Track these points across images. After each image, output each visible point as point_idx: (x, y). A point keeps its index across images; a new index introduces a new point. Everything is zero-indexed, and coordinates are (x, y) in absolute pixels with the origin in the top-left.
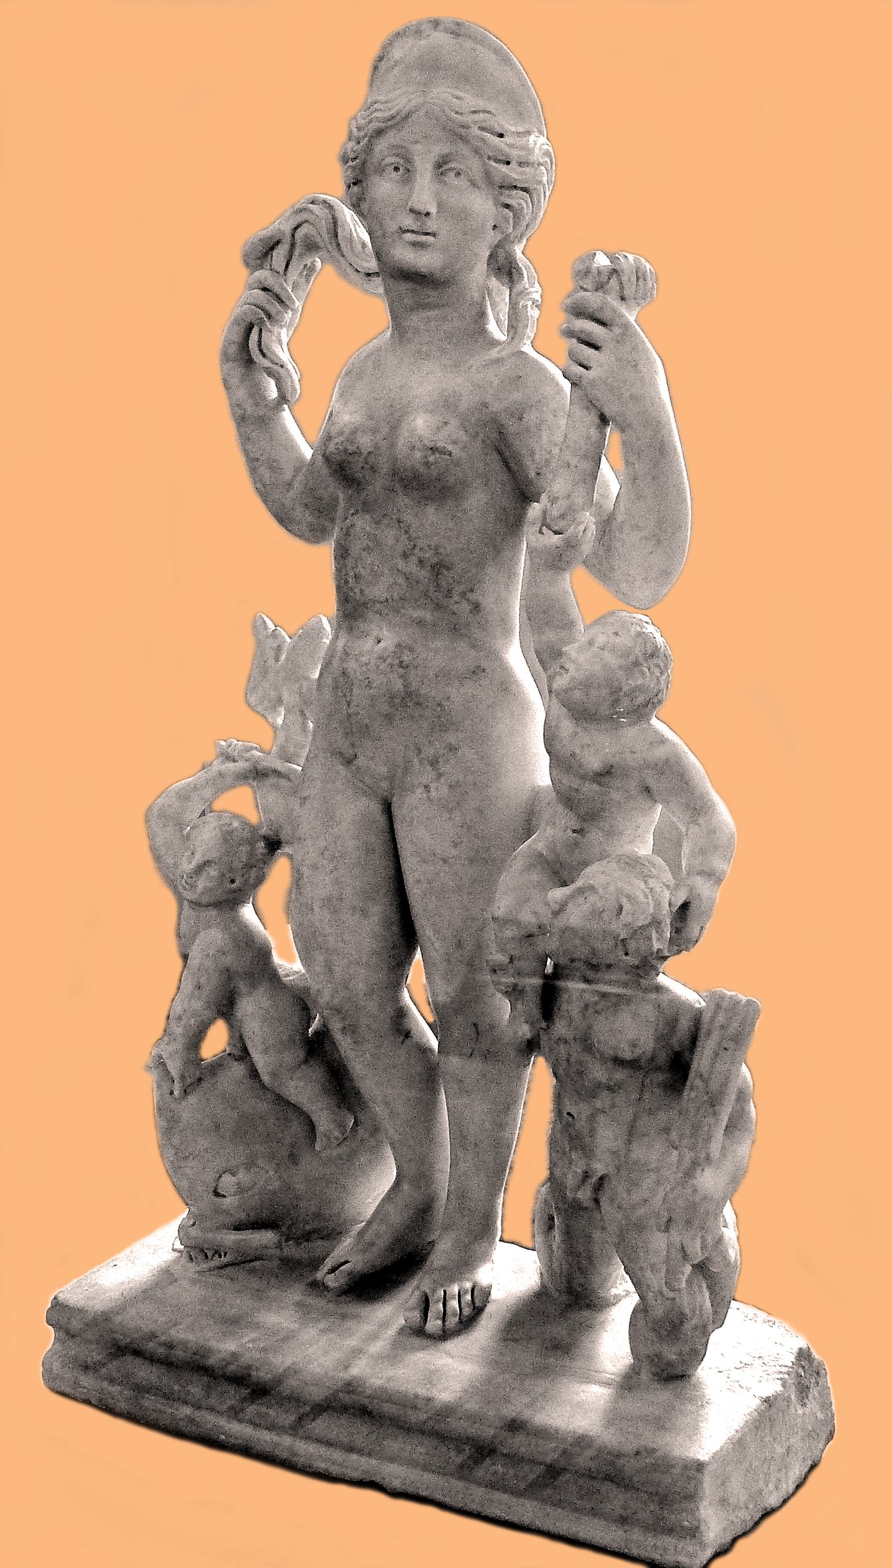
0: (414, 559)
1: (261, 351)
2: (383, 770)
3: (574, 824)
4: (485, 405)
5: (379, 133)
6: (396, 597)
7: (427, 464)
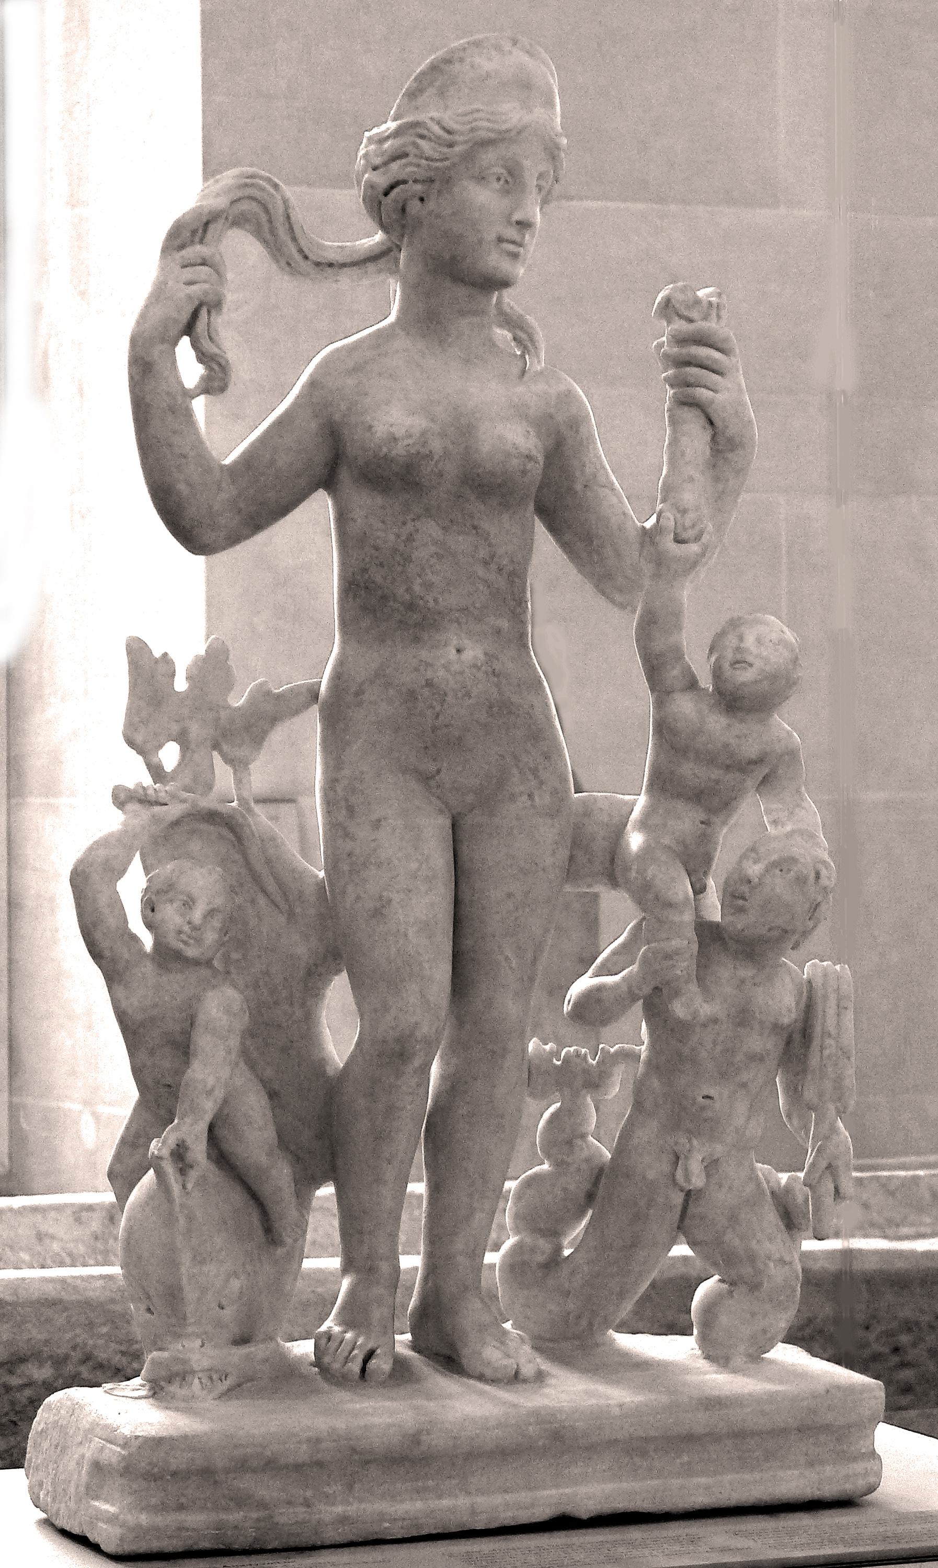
0: (493, 567)
1: (210, 337)
4: (551, 417)
5: (490, 143)
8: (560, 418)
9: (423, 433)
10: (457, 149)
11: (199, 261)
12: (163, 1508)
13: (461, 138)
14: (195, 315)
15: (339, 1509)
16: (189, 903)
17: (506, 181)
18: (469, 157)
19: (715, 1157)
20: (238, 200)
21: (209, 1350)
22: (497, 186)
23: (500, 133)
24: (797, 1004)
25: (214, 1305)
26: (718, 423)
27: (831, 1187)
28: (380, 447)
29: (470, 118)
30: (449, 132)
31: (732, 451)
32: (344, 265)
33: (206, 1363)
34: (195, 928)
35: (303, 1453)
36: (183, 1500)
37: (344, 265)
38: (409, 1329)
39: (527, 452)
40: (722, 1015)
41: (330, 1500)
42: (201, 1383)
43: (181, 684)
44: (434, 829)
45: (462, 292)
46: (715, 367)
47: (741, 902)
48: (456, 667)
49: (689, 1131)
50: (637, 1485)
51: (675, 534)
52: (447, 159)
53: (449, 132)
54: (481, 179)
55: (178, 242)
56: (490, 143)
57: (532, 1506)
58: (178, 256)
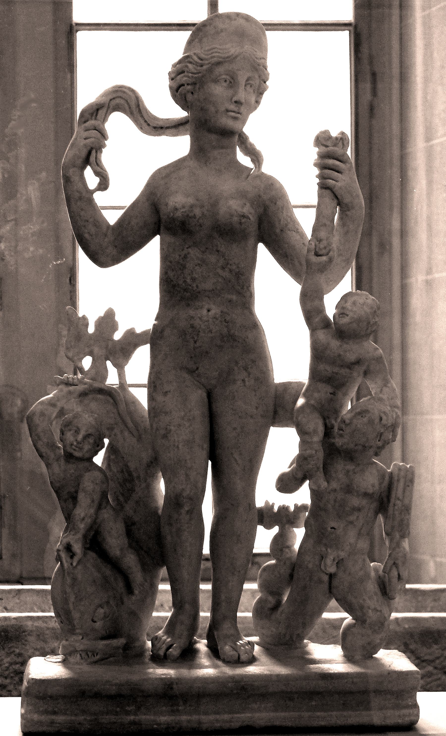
1: (96, 162)
2: (216, 374)
3: (330, 390)
4: (259, 196)
5: (219, 64)
6: (218, 288)
7: (241, 223)
8: (265, 197)
9: (192, 206)
10: (205, 67)
11: (93, 128)
12: (46, 712)
13: (206, 62)
14: (89, 153)
15: (132, 718)
16: (77, 431)
17: (231, 82)
18: (210, 71)
19: (341, 558)
20: (114, 99)
21: (85, 641)
22: (225, 84)
23: (224, 58)
24: (380, 484)
25: (89, 620)
26: (339, 197)
27: (396, 573)
28: (170, 213)
29: (210, 52)
30: (201, 60)
31: (349, 210)
32: (168, 128)
33: (82, 647)
34: (78, 443)
35: (113, 690)
36: (56, 709)
37: (168, 128)
38: (205, 635)
39: (242, 214)
40: (338, 488)
41: (128, 713)
42: (81, 656)
43: (91, 329)
44: (197, 396)
45: (213, 137)
46: (337, 169)
47: (341, 432)
48: (205, 319)
49: (325, 545)
50: (286, 714)
51: (316, 251)
52: (200, 73)
53: (201, 60)
54: (216, 81)
55: (83, 120)
56: (219, 64)
57: (231, 722)
58: (83, 126)
